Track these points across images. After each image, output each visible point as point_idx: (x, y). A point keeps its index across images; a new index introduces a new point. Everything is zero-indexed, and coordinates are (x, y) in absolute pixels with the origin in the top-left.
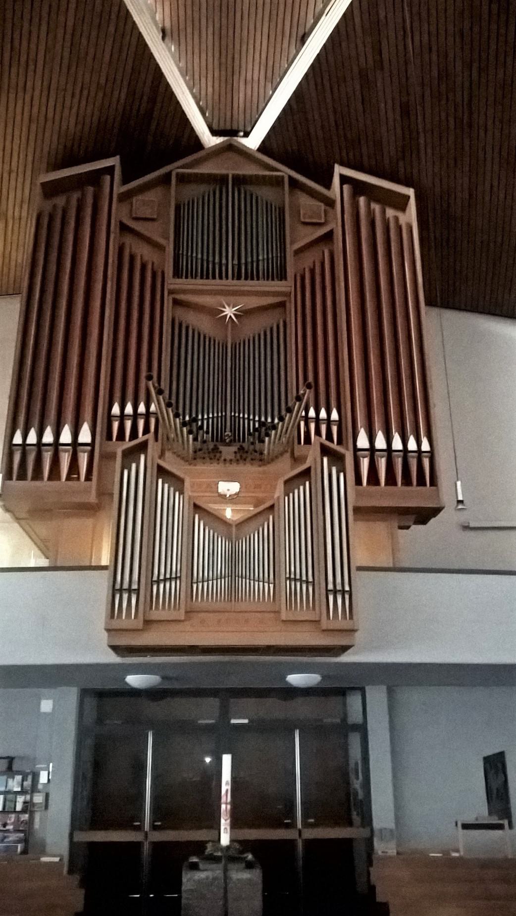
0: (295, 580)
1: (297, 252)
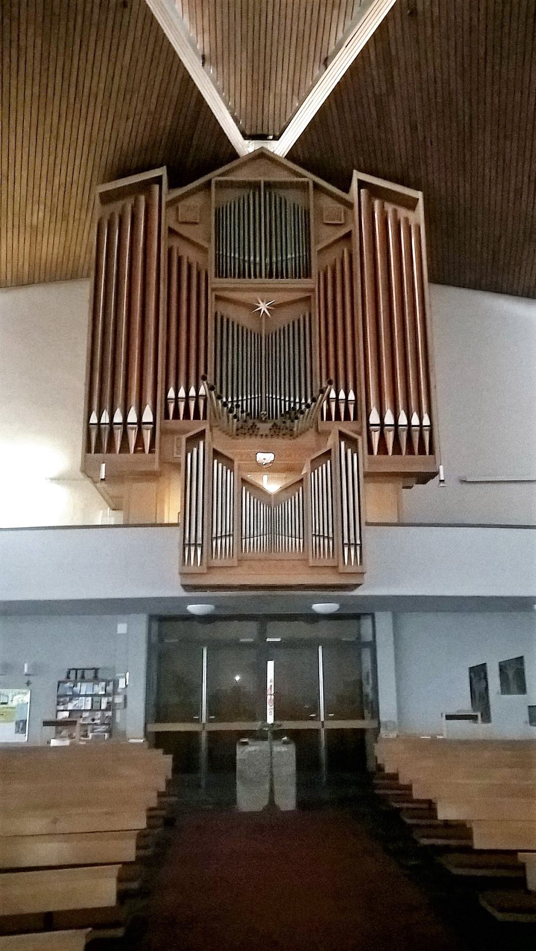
0: (319, 535)
1: (320, 252)
